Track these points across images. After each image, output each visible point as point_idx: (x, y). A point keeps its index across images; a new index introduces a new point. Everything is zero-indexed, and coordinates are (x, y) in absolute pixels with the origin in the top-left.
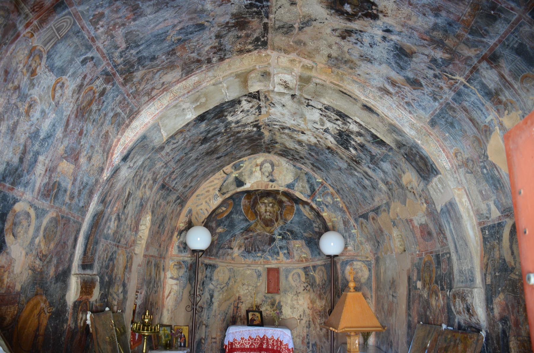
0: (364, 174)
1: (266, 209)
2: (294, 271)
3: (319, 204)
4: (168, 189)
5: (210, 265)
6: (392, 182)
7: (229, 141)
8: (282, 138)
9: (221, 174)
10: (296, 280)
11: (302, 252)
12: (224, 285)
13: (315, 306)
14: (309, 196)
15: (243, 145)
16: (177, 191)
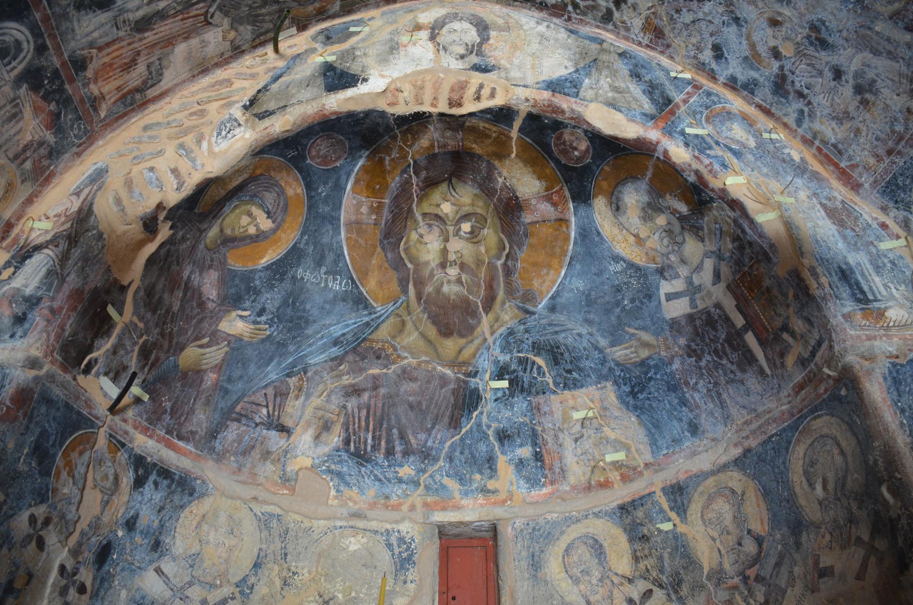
1: (444, 252)
2: (573, 532)
3: (700, 145)
5: (165, 473)
11: (603, 442)
12: (226, 591)
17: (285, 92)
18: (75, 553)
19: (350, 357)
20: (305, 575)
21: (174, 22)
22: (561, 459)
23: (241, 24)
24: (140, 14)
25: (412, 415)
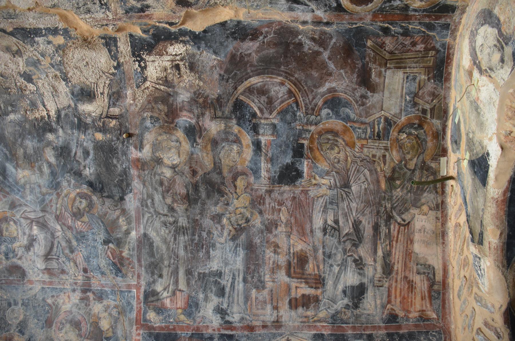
21: (396, 248)
23: (420, 200)
24: (379, 269)
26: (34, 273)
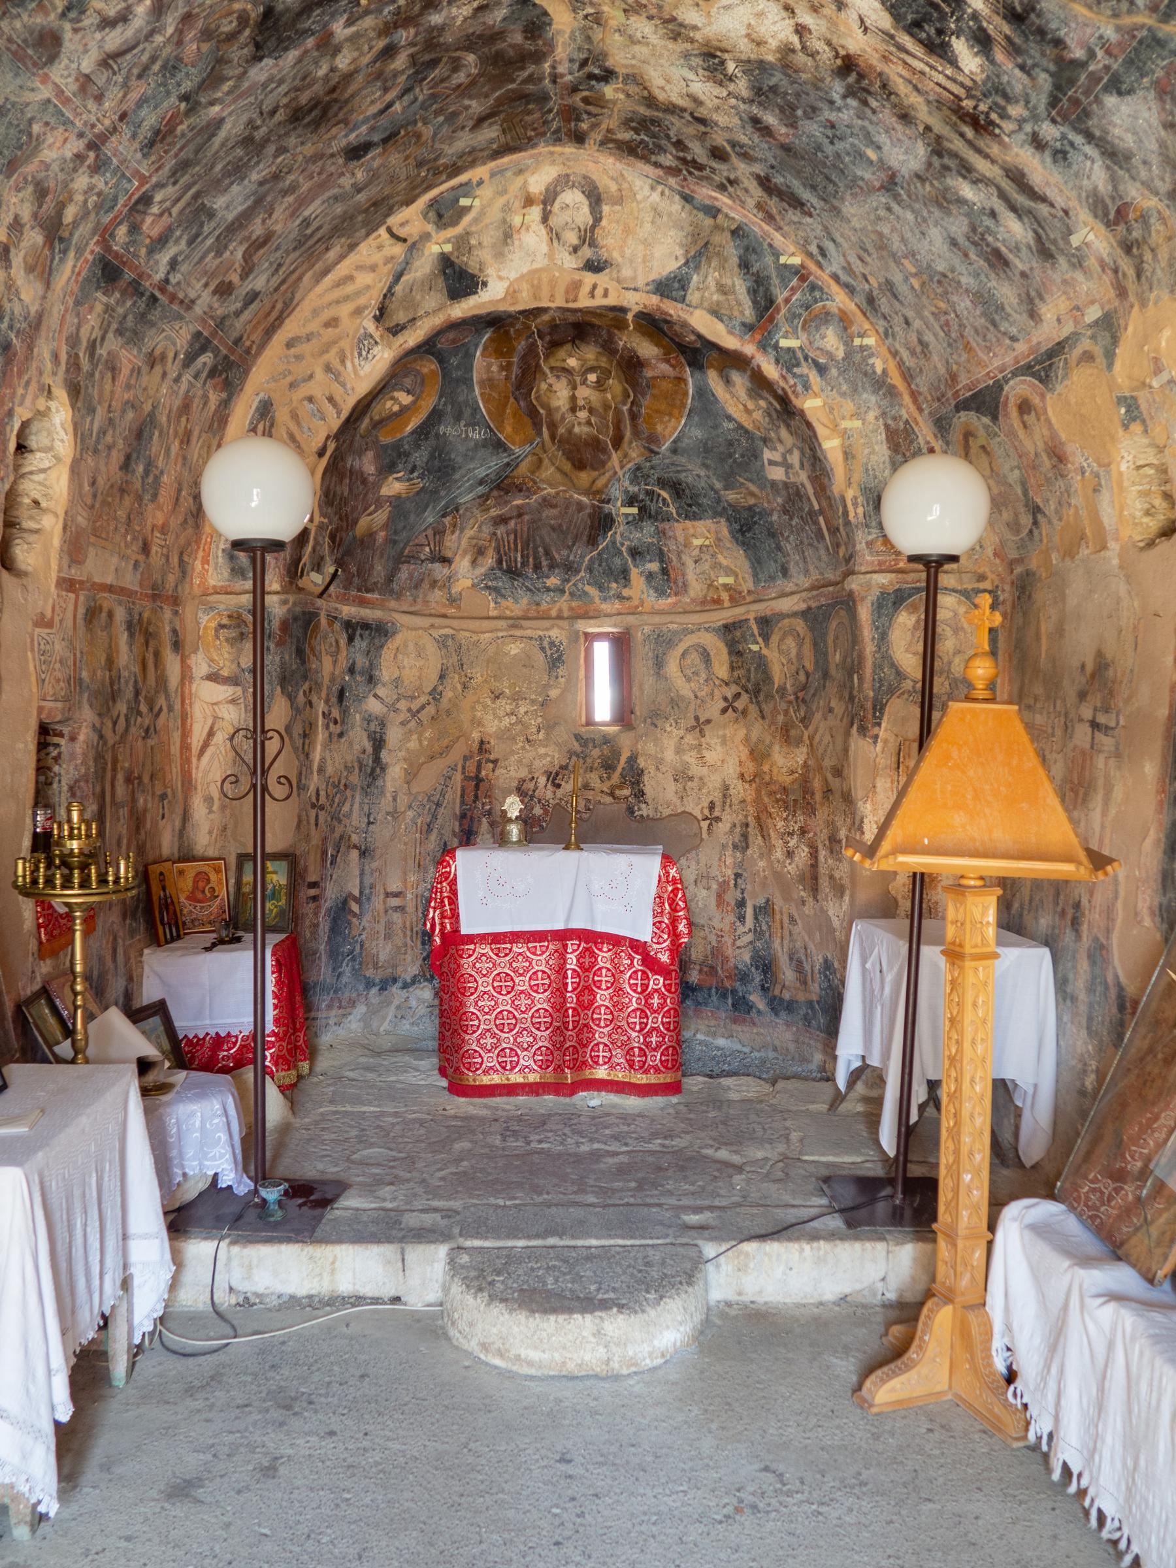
0: (1007, 185)
1: (573, 398)
3: (788, 360)
4: (135, 288)
5: (366, 626)
6: (1152, 203)
7: (389, 52)
8: (632, 41)
9: (380, 247)
10: (696, 673)
11: (716, 566)
12: (423, 699)
13: (766, 768)
14: (749, 328)
15: (464, 91)
16: (189, 305)
17: (409, 302)
18: (327, 701)
19: (495, 493)
20: (479, 678)
22: (683, 575)
25: (554, 535)
26: (67, 68)
